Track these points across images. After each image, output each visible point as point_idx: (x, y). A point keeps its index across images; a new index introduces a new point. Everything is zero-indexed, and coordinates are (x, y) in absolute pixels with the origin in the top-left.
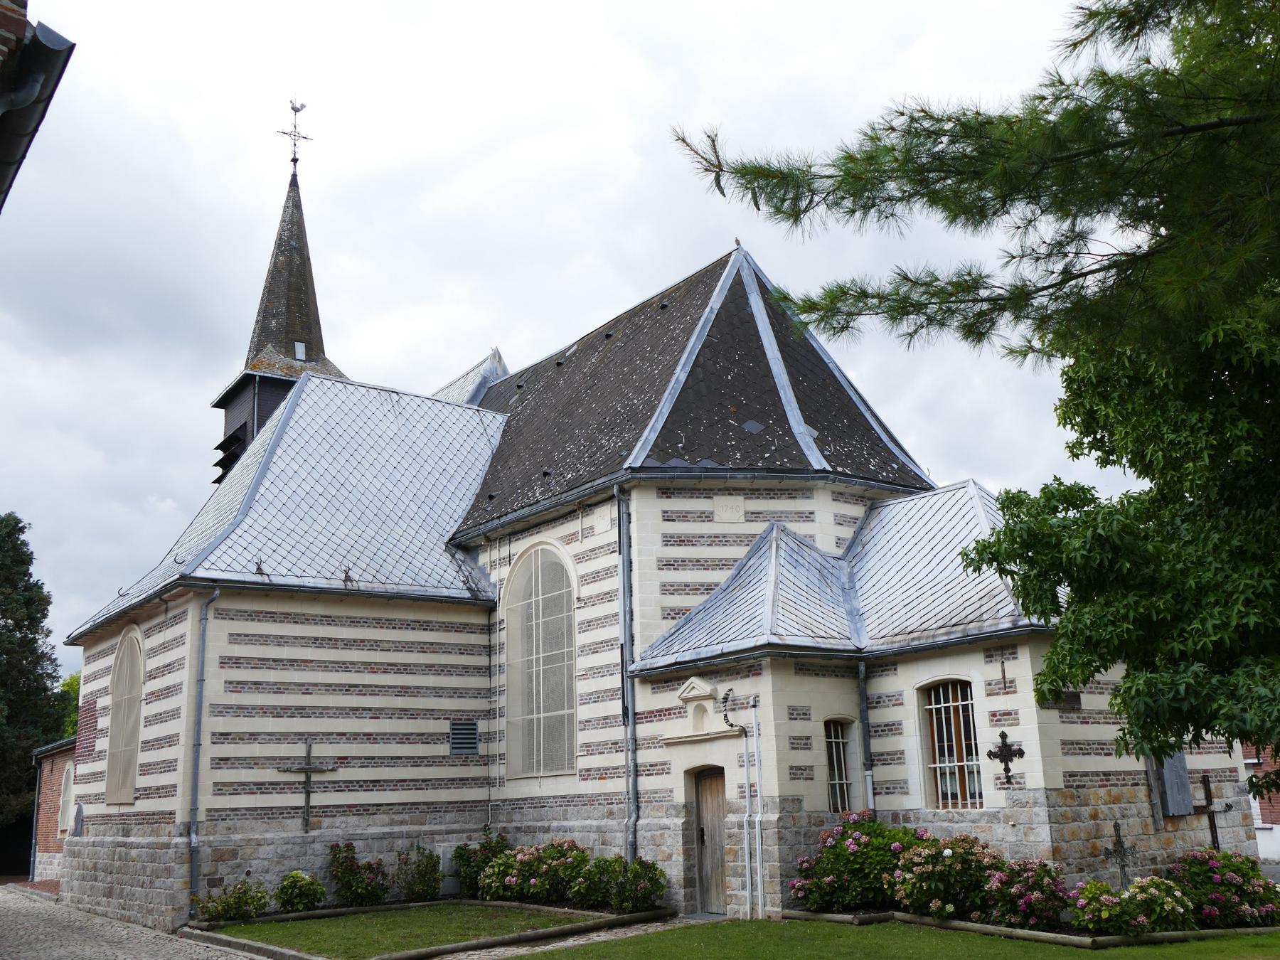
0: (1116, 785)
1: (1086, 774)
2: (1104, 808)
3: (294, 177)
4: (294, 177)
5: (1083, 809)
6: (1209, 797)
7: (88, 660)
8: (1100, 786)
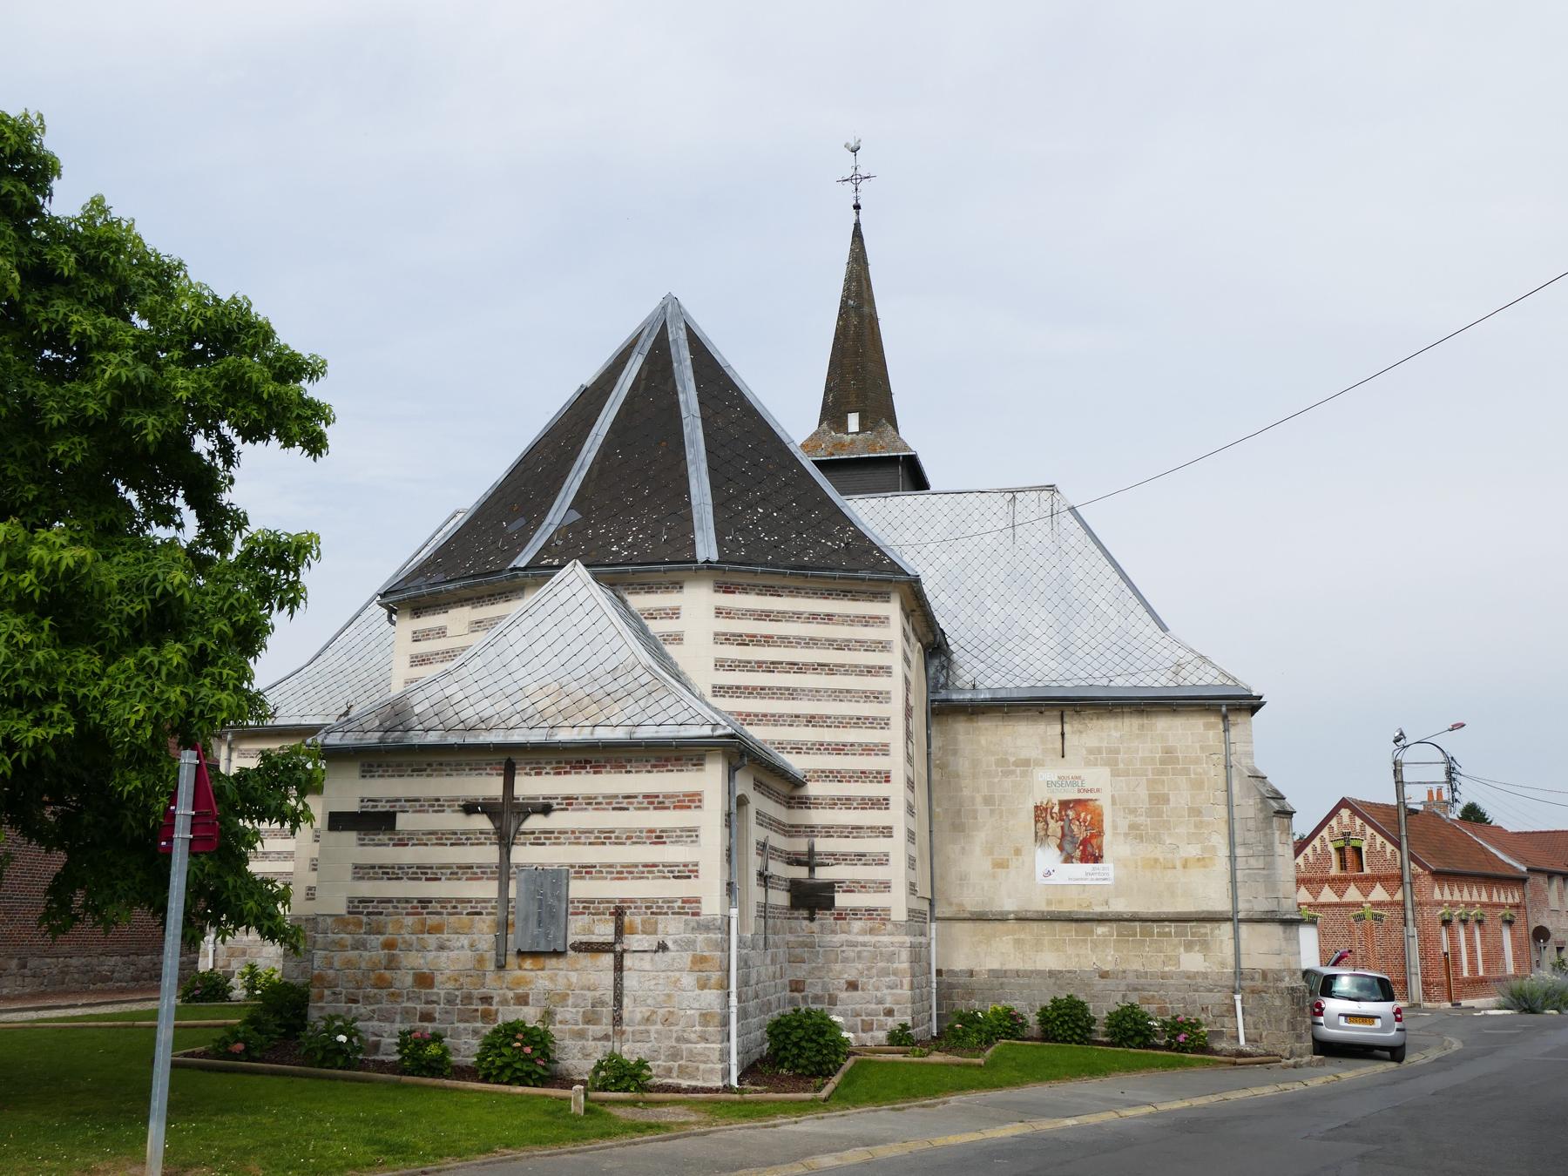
1: (389, 901)
3: (857, 226)
4: (857, 226)
6: (620, 931)
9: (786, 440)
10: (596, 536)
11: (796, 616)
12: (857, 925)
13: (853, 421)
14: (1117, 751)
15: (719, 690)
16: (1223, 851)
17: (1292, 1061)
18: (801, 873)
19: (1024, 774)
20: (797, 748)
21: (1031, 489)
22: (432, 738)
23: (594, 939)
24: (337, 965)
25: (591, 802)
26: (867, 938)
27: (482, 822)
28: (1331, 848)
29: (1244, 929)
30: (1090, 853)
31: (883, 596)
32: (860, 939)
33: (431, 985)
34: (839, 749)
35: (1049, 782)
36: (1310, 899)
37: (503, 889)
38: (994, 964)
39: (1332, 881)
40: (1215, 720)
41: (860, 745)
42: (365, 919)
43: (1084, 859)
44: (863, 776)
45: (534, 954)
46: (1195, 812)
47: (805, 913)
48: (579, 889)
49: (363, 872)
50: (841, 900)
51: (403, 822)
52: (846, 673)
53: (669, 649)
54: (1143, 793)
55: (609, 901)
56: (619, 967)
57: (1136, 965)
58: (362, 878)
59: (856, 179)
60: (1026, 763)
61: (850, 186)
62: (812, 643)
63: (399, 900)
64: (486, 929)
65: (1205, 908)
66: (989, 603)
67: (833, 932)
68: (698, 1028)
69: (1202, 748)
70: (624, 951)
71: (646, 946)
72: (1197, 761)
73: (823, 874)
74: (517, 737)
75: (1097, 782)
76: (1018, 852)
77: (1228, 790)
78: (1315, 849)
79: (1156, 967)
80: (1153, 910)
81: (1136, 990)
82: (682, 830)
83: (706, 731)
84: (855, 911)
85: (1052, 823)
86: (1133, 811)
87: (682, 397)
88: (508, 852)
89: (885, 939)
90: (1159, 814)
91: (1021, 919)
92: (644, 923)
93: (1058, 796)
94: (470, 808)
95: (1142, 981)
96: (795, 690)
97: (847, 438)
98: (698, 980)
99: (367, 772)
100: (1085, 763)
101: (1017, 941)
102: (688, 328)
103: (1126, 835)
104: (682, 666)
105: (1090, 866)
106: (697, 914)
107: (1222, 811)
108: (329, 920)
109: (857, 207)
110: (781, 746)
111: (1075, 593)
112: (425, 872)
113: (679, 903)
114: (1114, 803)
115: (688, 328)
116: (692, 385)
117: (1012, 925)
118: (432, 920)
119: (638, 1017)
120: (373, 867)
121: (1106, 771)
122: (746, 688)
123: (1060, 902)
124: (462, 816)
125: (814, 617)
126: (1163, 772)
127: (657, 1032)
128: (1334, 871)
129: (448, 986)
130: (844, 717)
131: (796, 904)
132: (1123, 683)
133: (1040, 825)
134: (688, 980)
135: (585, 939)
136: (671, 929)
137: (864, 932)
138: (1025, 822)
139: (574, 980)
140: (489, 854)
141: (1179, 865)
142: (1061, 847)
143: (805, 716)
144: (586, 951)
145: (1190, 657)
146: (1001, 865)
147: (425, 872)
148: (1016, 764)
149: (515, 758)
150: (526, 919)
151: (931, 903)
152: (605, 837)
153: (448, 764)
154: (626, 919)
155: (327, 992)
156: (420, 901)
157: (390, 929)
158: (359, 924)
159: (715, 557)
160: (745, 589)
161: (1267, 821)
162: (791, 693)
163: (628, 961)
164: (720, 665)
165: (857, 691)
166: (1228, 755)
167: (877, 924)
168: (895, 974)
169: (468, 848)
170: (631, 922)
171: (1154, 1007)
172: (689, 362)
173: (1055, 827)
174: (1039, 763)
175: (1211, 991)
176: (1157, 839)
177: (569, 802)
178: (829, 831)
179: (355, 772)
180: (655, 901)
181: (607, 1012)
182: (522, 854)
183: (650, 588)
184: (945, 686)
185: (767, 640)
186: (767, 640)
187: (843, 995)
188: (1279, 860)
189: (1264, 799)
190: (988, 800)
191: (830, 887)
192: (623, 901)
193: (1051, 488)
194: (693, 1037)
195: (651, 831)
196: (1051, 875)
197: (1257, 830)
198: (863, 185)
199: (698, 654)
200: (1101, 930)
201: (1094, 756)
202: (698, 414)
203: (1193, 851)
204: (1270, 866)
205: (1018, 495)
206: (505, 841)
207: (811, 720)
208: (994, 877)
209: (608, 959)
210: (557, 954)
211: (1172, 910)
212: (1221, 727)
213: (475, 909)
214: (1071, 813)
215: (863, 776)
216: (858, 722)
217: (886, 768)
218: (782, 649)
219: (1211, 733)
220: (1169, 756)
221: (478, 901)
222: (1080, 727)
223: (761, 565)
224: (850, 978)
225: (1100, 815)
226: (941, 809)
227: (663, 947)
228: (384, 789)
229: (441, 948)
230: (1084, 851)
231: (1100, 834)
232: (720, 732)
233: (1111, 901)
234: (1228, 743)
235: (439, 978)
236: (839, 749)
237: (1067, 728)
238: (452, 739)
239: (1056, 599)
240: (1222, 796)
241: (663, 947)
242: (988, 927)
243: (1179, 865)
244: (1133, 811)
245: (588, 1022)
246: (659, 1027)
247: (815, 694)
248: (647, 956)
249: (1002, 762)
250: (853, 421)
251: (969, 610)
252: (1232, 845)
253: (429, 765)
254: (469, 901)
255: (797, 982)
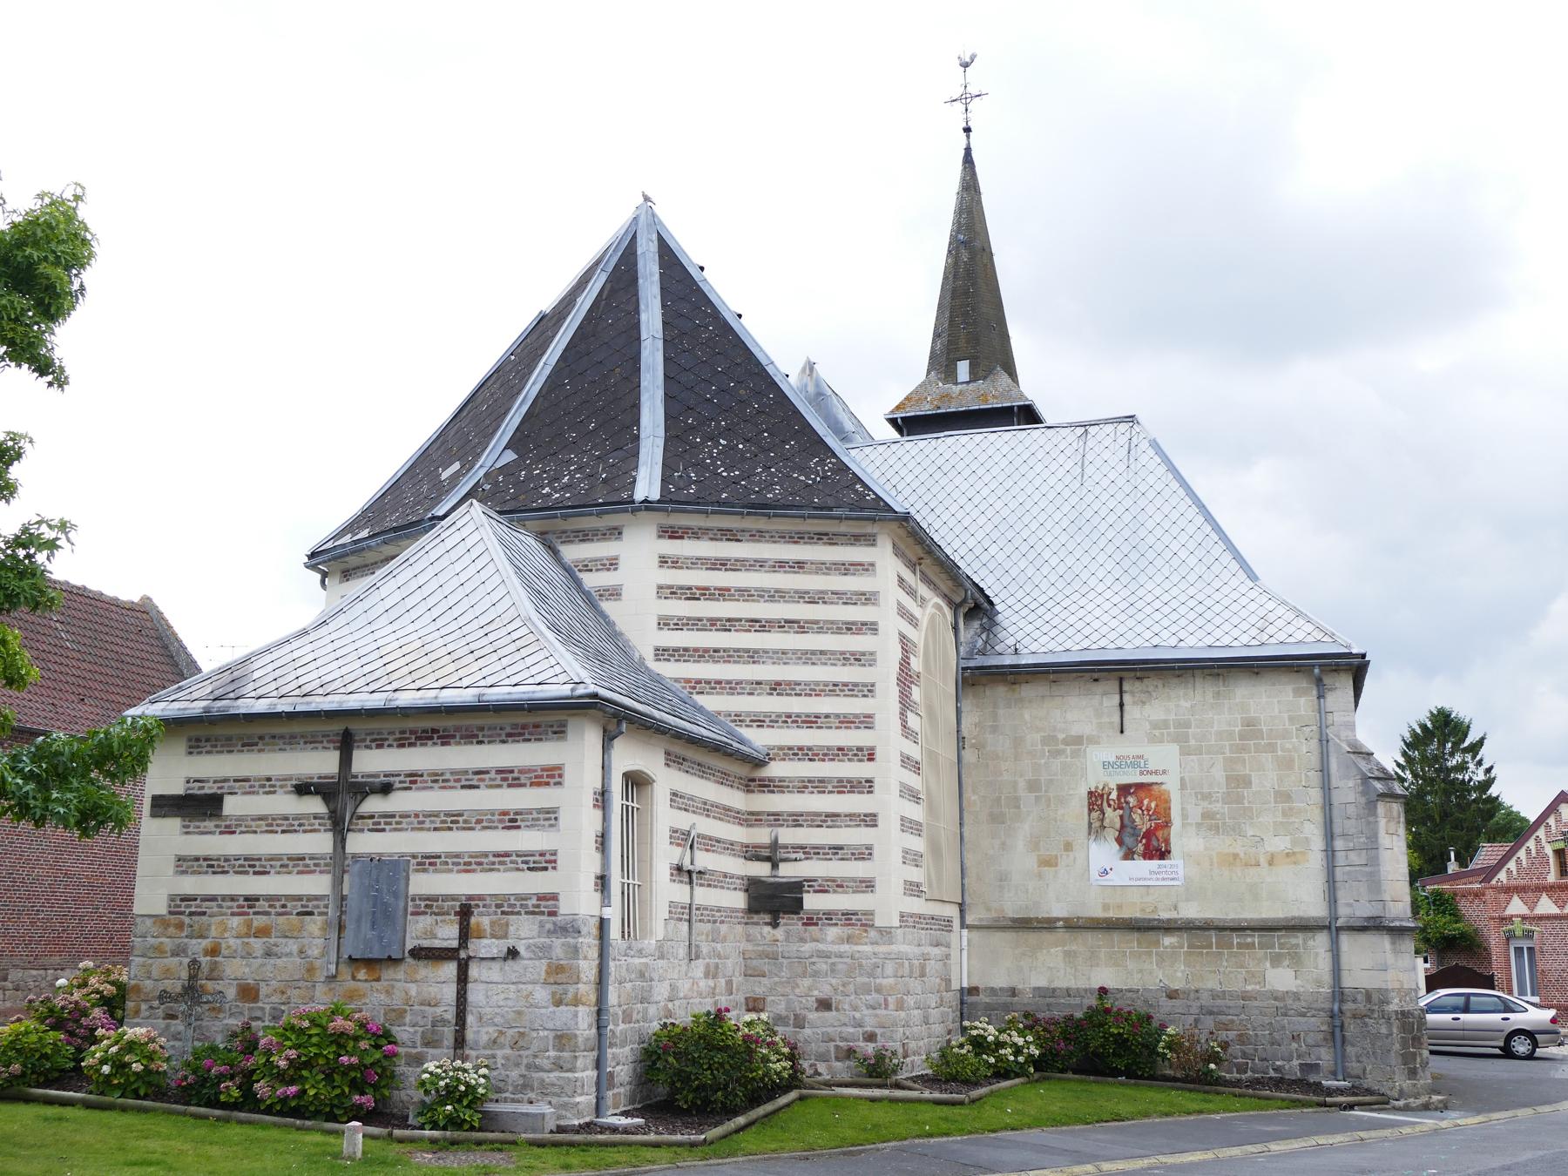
0: (267, 914)
1: (213, 898)
2: (232, 941)
3: (968, 150)
4: (968, 150)
5: (194, 941)
6: (465, 935)
7: (1433, 983)
8: (233, 914)
9: (764, 362)
10: (529, 477)
11: (759, 564)
12: (832, 932)
13: (963, 369)
14: (1187, 725)
15: (663, 653)
16: (1318, 843)
17: (1401, 1103)
18: (761, 870)
19: (1075, 754)
20: (759, 721)
21: (1107, 421)
22: (261, 706)
23: (437, 944)
24: (155, 974)
25: (438, 779)
26: (845, 948)
27: (315, 805)
28: (1549, 850)
29: (1345, 940)
30: (1157, 850)
31: (870, 540)
32: (835, 948)
33: (256, 999)
34: (811, 721)
35: (1103, 764)
36: (1524, 910)
37: (338, 883)
38: (1041, 981)
39: (1550, 889)
40: (1304, 683)
41: (837, 716)
42: (187, 920)
43: (1149, 854)
44: (841, 753)
45: (370, 963)
46: (1284, 796)
47: (767, 918)
48: (422, 884)
49: (186, 864)
50: (811, 902)
51: (231, 806)
52: (820, 631)
53: (606, 606)
54: (1219, 774)
55: (453, 898)
56: (463, 979)
57: (1211, 983)
58: (183, 872)
59: (966, 99)
60: (1078, 740)
61: (959, 106)
62: (777, 595)
63: (224, 898)
64: (317, 932)
65: (1296, 913)
66: (1047, 554)
67: (802, 940)
68: (552, 1053)
69: (1291, 719)
70: (470, 958)
71: (494, 952)
72: (1285, 735)
73: (788, 871)
74: (353, 702)
75: (1163, 763)
76: (1068, 847)
77: (1324, 770)
78: (1529, 851)
79: (1236, 984)
80: (1232, 916)
81: (1211, 1013)
82: (539, 811)
83: (566, 690)
84: (829, 916)
85: (1109, 812)
86: (1207, 797)
87: (643, 317)
88: (343, 840)
89: (867, 948)
90: (1240, 799)
91: (1074, 926)
92: (492, 924)
93: (1114, 781)
94: (303, 789)
95: (1219, 1002)
96: (756, 651)
97: (956, 389)
98: (554, 994)
99: (196, 746)
100: (1150, 744)
101: (1067, 954)
102: (661, 239)
103: (1199, 825)
104: (621, 626)
105: (1155, 863)
106: (553, 914)
107: (1315, 795)
108: (149, 922)
109: (967, 130)
110: (738, 718)
111: (1151, 540)
112: (253, 865)
113: (534, 901)
114: (1183, 786)
115: (661, 239)
116: (657, 303)
117: (1061, 934)
118: (258, 921)
119: (484, 1038)
120: (197, 859)
121: (1175, 748)
122: (696, 650)
123: (1120, 907)
124: (293, 797)
125: (781, 565)
126: (1244, 749)
127: (507, 1058)
128: (1552, 878)
129: (274, 999)
130: (817, 683)
131: (754, 908)
132: (1194, 644)
133: (1095, 815)
134: (542, 994)
135: (426, 943)
136: (524, 931)
137: (841, 941)
138: (1077, 809)
139: (413, 993)
140: (320, 843)
141: (1263, 860)
142: (1120, 841)
143: (767, 683)
144: (427, 958)
145: (1281, 610)
146: (1048, 862)
147: (253, 865)
148: (1066, 742)
149: (355, 726)
150: (359, 920)
151: (962, 907)
152: (453, 821)
153: (282, 737)
154: (473, 920)
155: (144, 1007)
156: (247, 899)
157: (213, 933)
158: (180, 926)
159: (655, 495)
160: (696, 534)
161: (1371, 807)
162: (753, 656)
163: (474, 971)
164: (664, 623)
165: (833, 653)
166: (1322, 728)
167: (856, 931)
168: (878, 990)
169: (301, 836)
170: (478, 924)
171: (1232, 1035)
172: (657, 277)
173: (1112, 816)
174: (1093, 740)
175: (1303, 1015)
176: (1236, 830)
177: (413, 779)
178: (797, 820)
179: (181, 747)
180: (506, 897)
181: (448, 1033)
182: (361, 843)
183: (585, 536)
184: (983, 653)
185: (723, 593)
186: (723, 593)
187: (813, 1016)
188: (1385, 856)
189: (1365, 779)
190: (1033, 786)
191: (797, 887)
192: (470, 897)
193: (1131, 419)
194: (546, 1063)
195: (505, 813)
196: (1108, 875)
197: (1359, 817)
198: (975, 105)
199: (640, 616)
200: (1168, 940)
201: (1158, 732)
202: (660, 335)
203: (1280, 844)
204: (1374, 862)
205: (1092, 430)
206: (339, 826)
207: (776, 688)
208: (1040, 876)
209: (450, 969)
210: (393, 961)
211: (1255, 916)
212: (1315, 692)
213: (306, 907)
214: (1132, 800)
215: (841, 753)
216: (835, 689)
217: (869, 744)
218: (741, 604)
219: (1303, 700)
220: (1251, 728)
221: (311, 898)
222: (1143, 697)
223: (712, 504)
224: (821, 996)
225: (1168, 801)
226: (974, 799)
227: (513, 954)
228: (213, 767)
229: (268, 954)
230: (1147, 846)
231: (1167, 824)
232: (581, 691)
233: (1181, 905)
234: (1321, 712)
235: (264, 990)
236: (811, 721)
237: (1126, 698)
238: (284, 706)
239: (1126, 548)
240: (1315, 777)
241: (513, 954)
242: (1032, 937)
243: (1263, 860)
244: (1207, 797)
245: (427, 1044)
246: (508, 1051)
247: (781, 656)
248: (496, 966)
249: (1049, 740)
250: (963, 369)
251: (1023, 564)
252: (1329, 836)
253: (261, 738)
254: (299, 898)
255: (755, 1000)
